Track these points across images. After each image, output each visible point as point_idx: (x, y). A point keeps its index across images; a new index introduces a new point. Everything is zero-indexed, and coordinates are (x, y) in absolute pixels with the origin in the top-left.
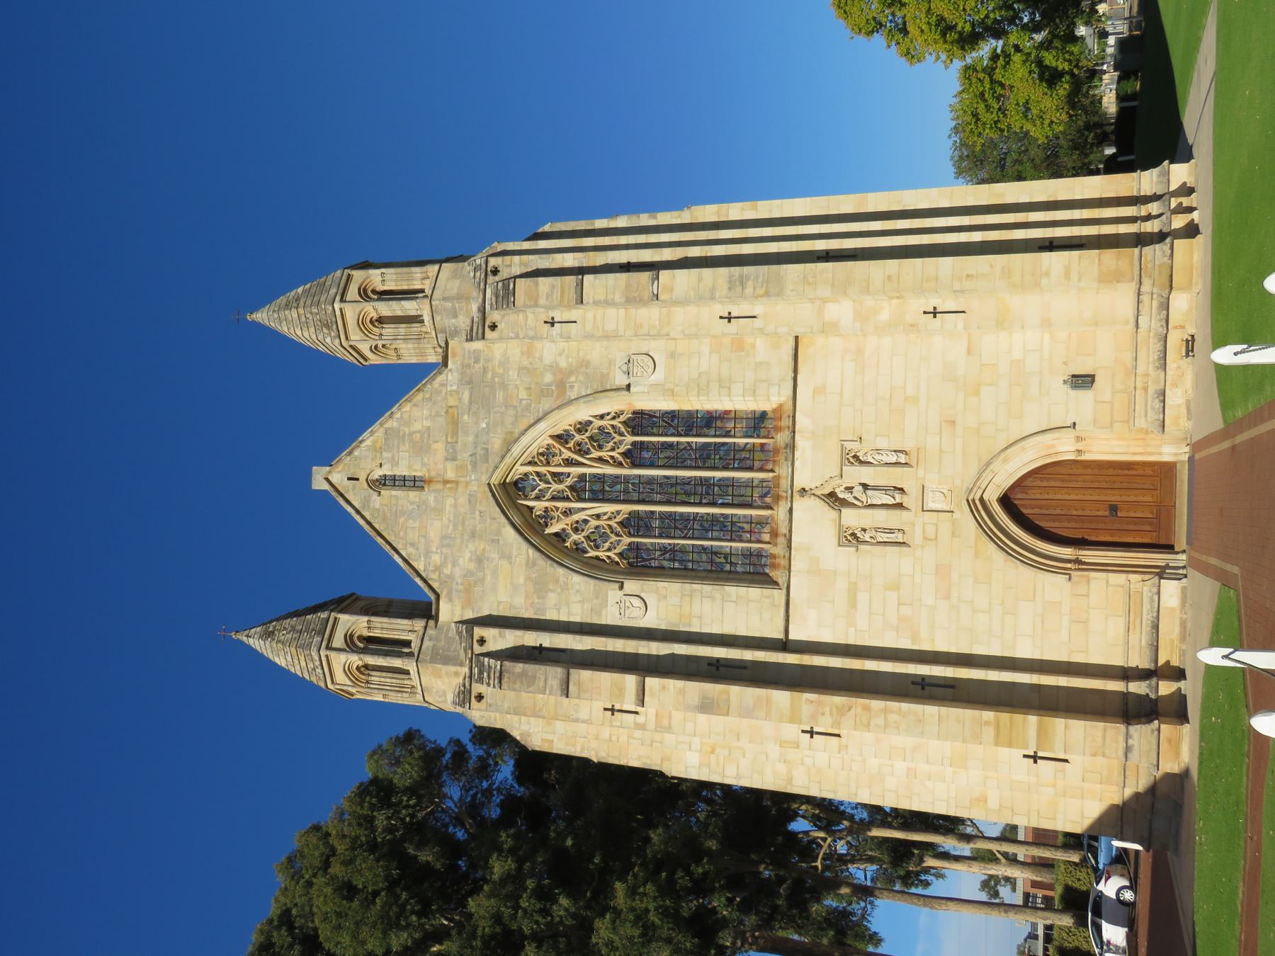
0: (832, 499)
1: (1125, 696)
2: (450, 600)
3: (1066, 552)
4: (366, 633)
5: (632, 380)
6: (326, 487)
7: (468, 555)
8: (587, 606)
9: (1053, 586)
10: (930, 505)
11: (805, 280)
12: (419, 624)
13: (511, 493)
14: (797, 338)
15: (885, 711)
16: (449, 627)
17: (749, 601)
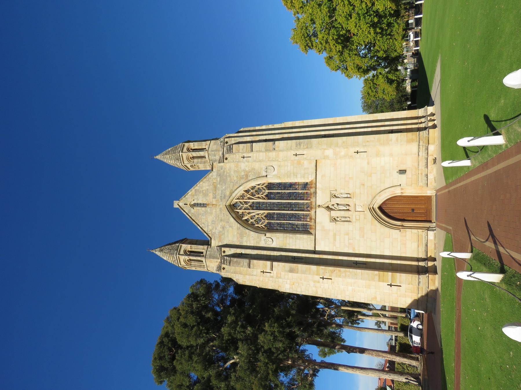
2: (215, 240)
3: (399, 223)
4: (190, 250)
5: (267, 174)
9: (395, 233)
12: (206, 247)
13: (232, 208)
15: (345, 271)
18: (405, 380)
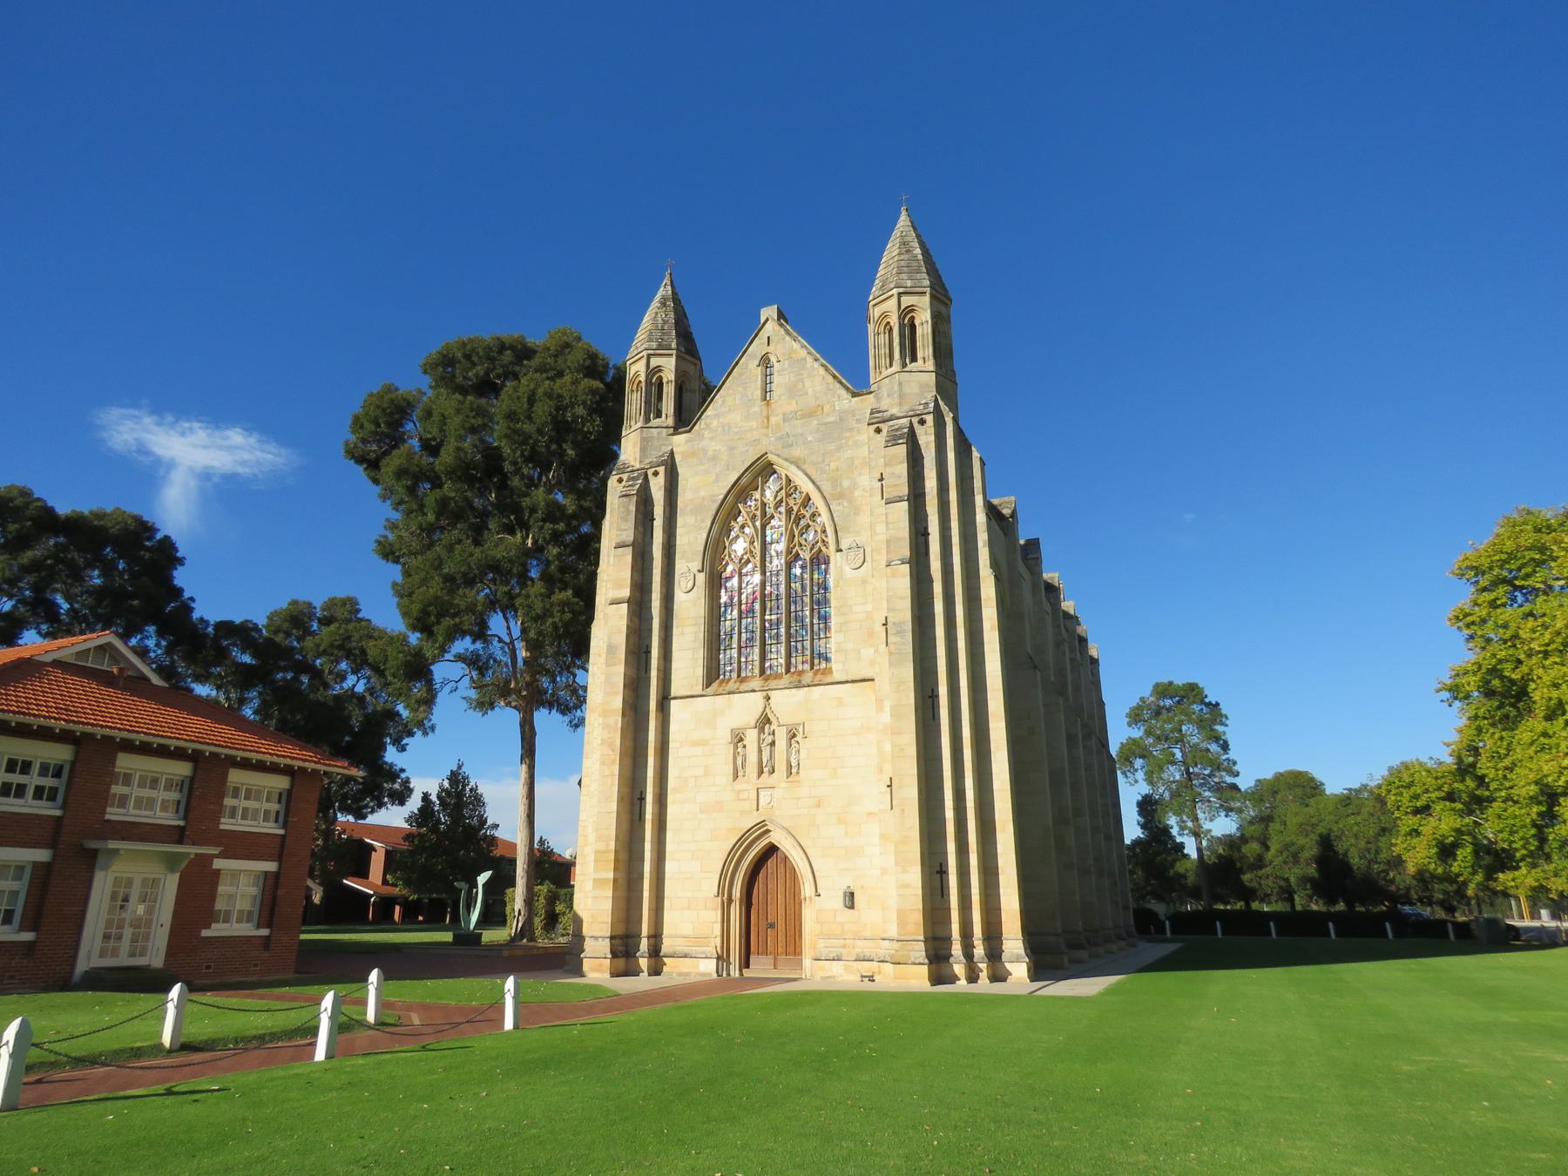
0: (764, 722)
1: (639, 936)
3: (737, 892)
4: (917, 322)
9: (711, 884)
12: (671, 422)
13: (763, 469)
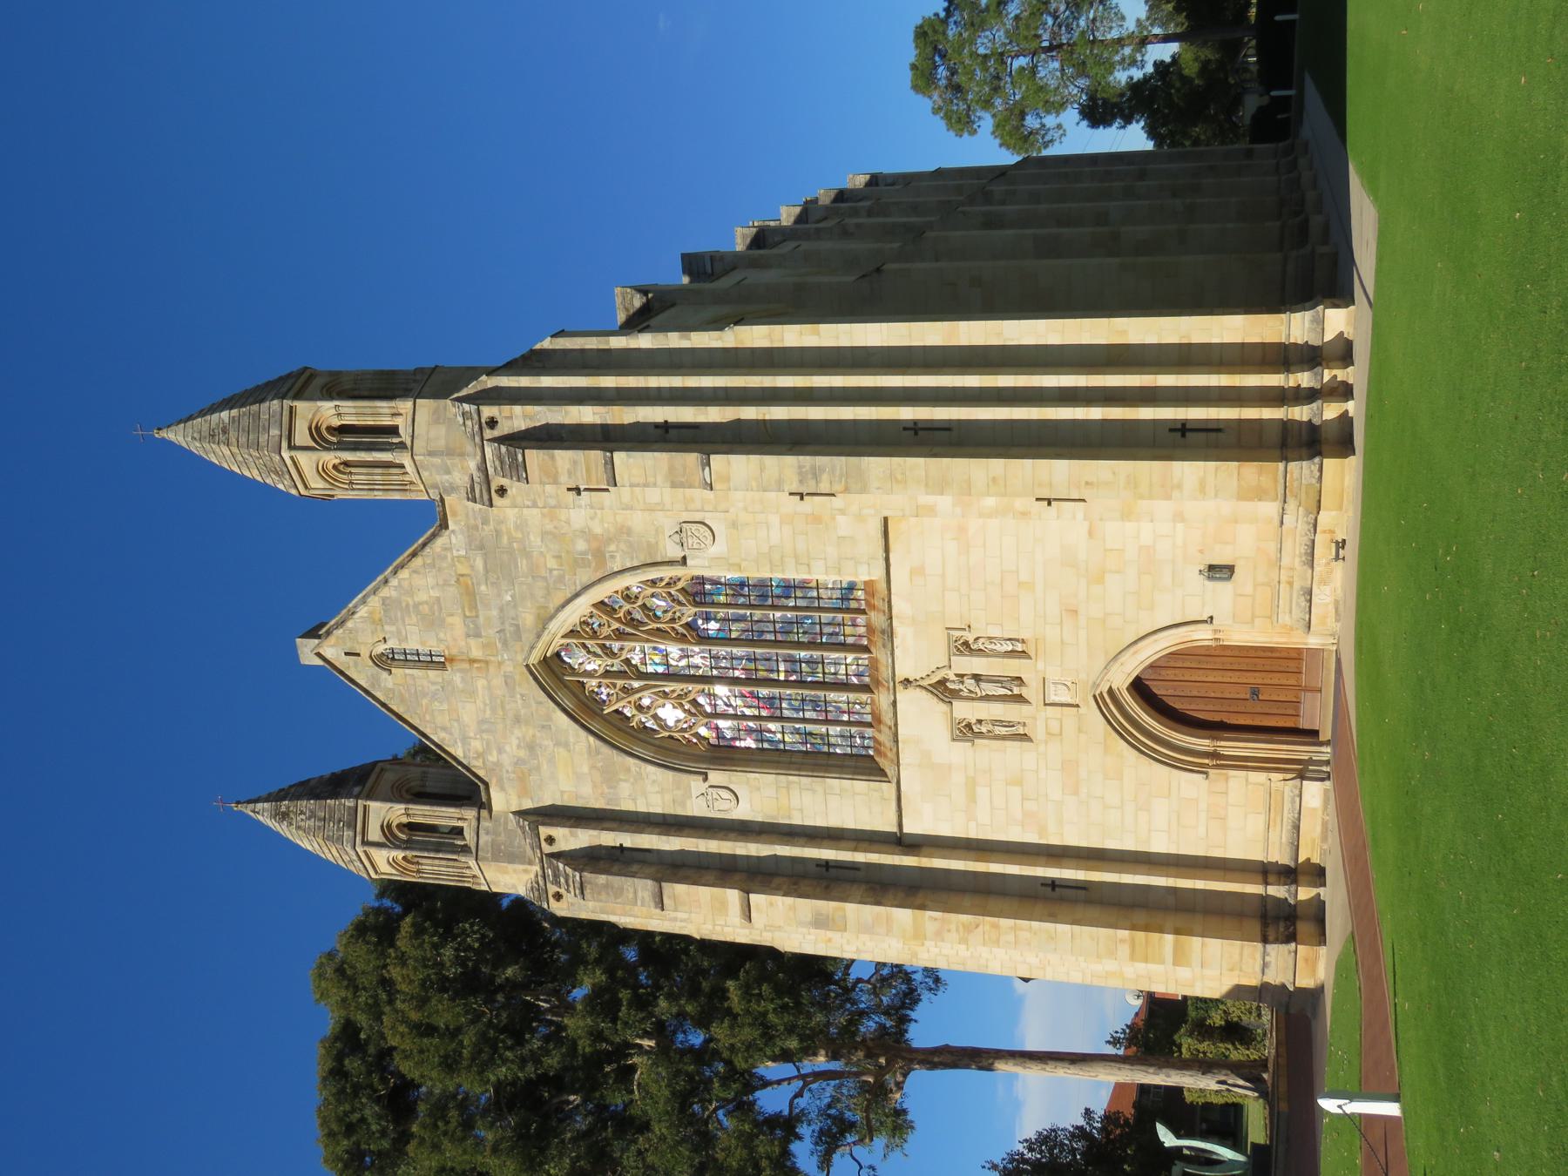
0: (942, 690)
1: (1264, 899)
2: (502, 789)
4: (336, 422)
5: (687, 553)
6: (320, 662)
7: (515, 742)
8: (668, 797)
9: (1189, 784)
10: (1052, 698)
11: (892, 476)
12: (470, 813)
14: (886, 519)
15: (1014, 929)
16: (506, 818)
17: (855, 794)
18: (1216, 1087)
